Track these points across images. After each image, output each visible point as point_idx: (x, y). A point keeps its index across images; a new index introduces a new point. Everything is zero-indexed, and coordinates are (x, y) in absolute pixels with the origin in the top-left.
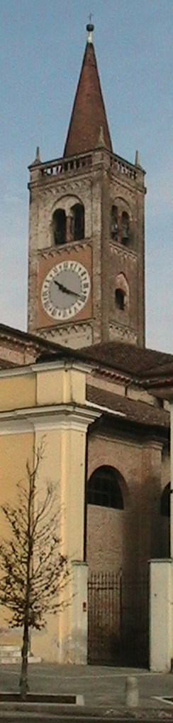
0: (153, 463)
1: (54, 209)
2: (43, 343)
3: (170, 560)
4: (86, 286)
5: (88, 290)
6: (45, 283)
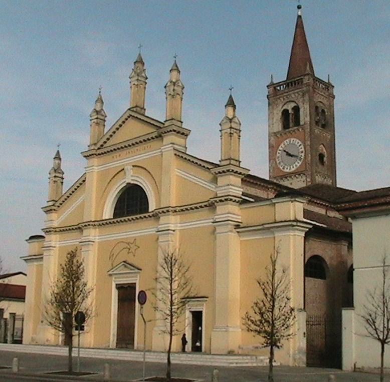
1: (282, 109)
4: (302, 152)
5: (303, 154)
6: (278, 151)
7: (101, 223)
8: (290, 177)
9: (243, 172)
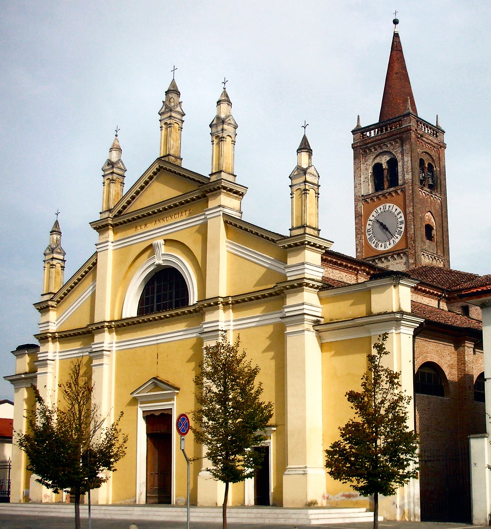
0: (466, 359)
1: (373, 164)
2: (371, 267)
3: (481, 351)
4: (401, 223)
5: (403, 226)
6: (369, 222)
7: (119, 323)
8: (386, 258)
9: (324, 244)
